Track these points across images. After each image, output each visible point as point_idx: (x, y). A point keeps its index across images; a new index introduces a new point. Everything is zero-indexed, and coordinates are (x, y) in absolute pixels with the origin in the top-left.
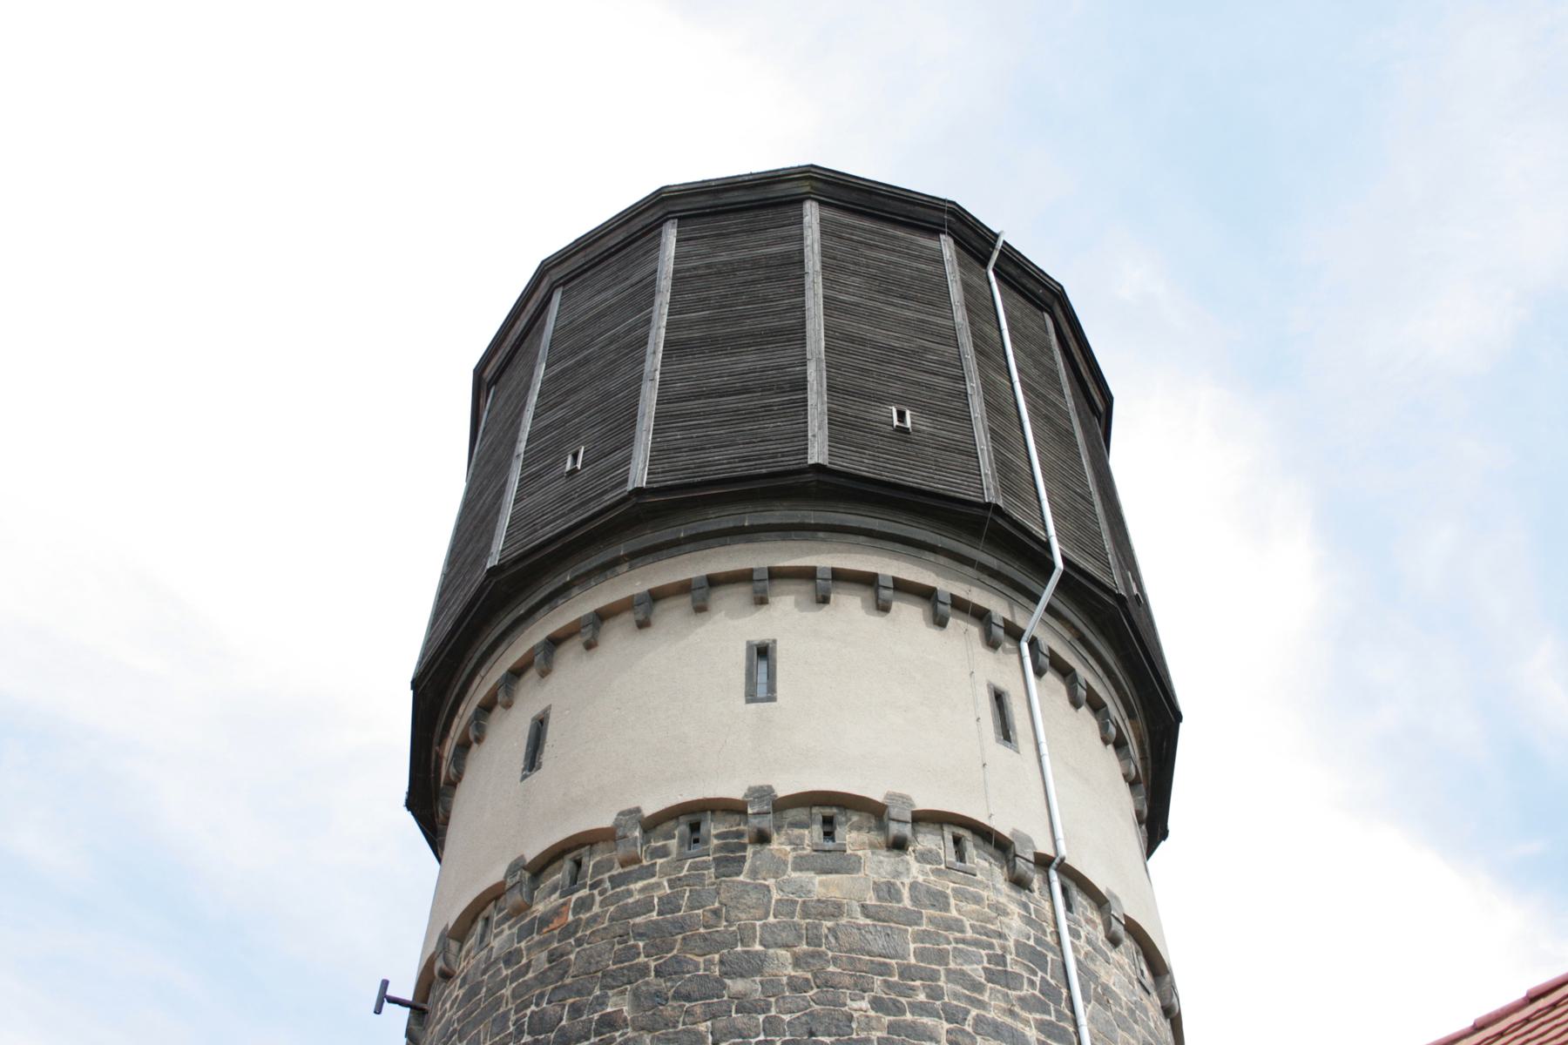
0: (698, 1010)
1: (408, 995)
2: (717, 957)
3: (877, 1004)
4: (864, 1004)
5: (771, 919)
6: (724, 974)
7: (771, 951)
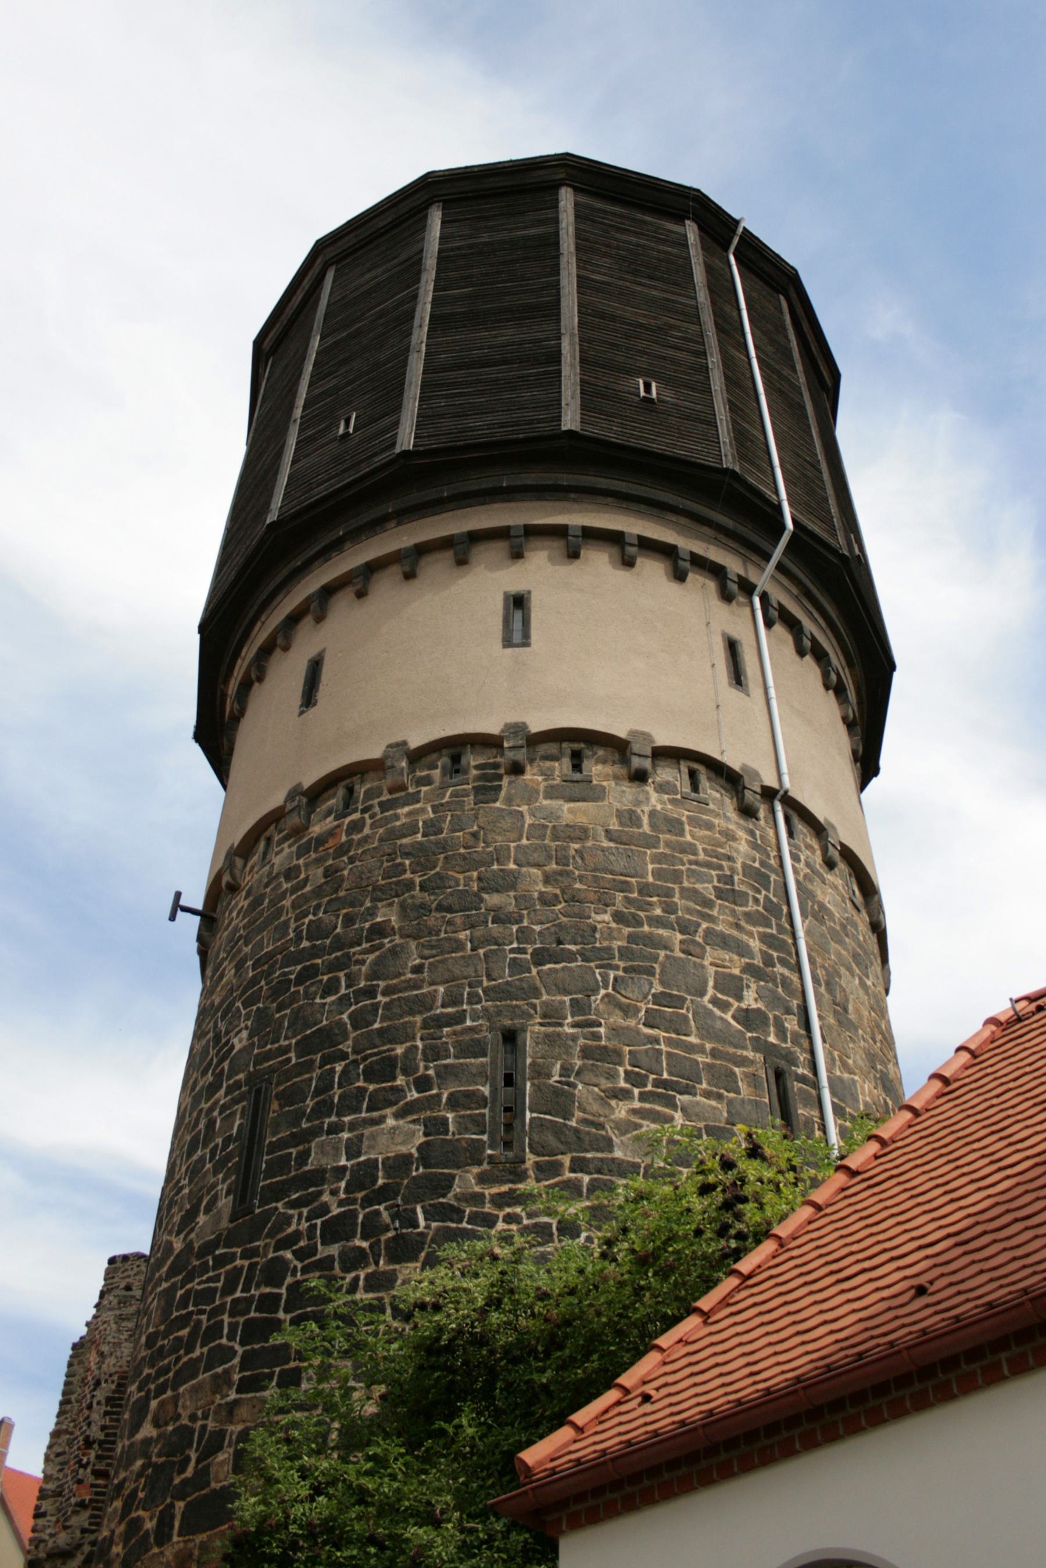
3: (618, 917)
4: (607, 917)
5: (524, 842)
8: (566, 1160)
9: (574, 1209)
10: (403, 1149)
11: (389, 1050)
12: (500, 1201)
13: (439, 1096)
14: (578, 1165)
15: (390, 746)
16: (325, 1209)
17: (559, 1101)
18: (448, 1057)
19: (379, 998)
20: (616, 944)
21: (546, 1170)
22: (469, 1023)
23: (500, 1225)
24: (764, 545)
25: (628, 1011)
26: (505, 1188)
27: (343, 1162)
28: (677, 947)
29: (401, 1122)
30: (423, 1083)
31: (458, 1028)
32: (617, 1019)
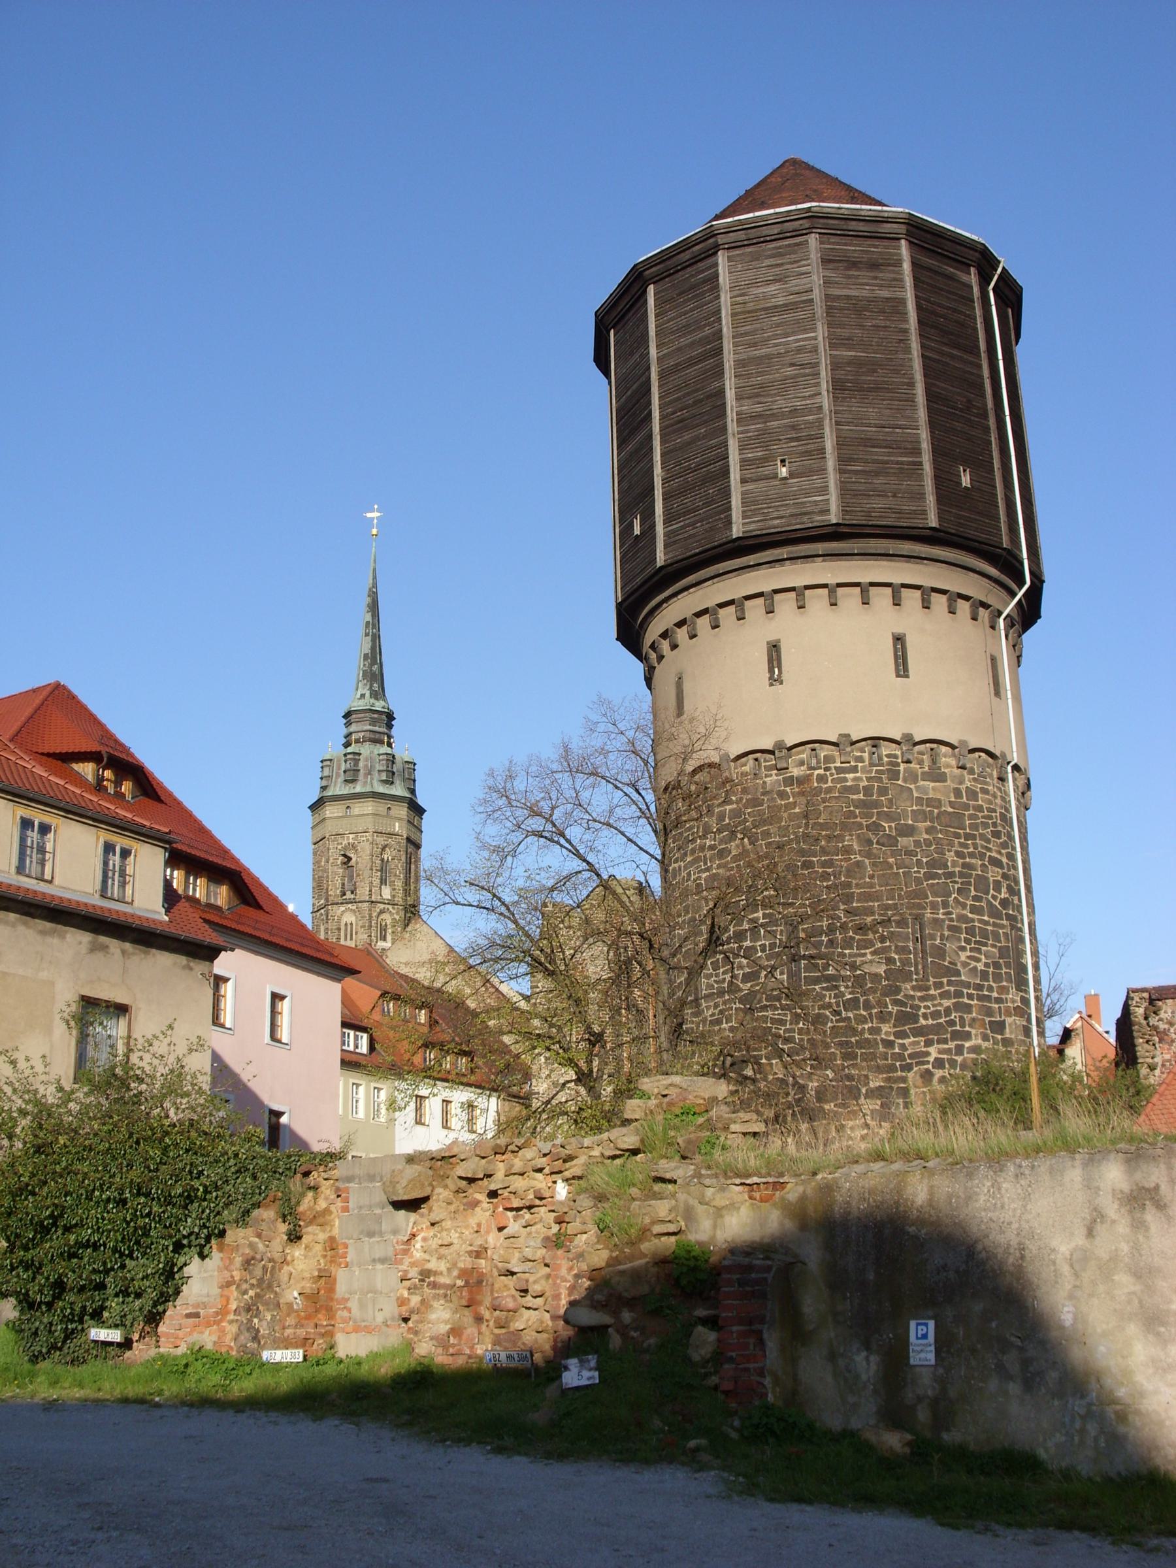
3: (958, 854)
4: (952, 853)
8: (945, 980)
9: (947, 1003)
12: (922, 999)
14: (950, 983)
20: (957, 869)
21: (938, 985)
23: (923, 1010)
24: (1014, 587)
25: (964, 906)
32: (959, 910)
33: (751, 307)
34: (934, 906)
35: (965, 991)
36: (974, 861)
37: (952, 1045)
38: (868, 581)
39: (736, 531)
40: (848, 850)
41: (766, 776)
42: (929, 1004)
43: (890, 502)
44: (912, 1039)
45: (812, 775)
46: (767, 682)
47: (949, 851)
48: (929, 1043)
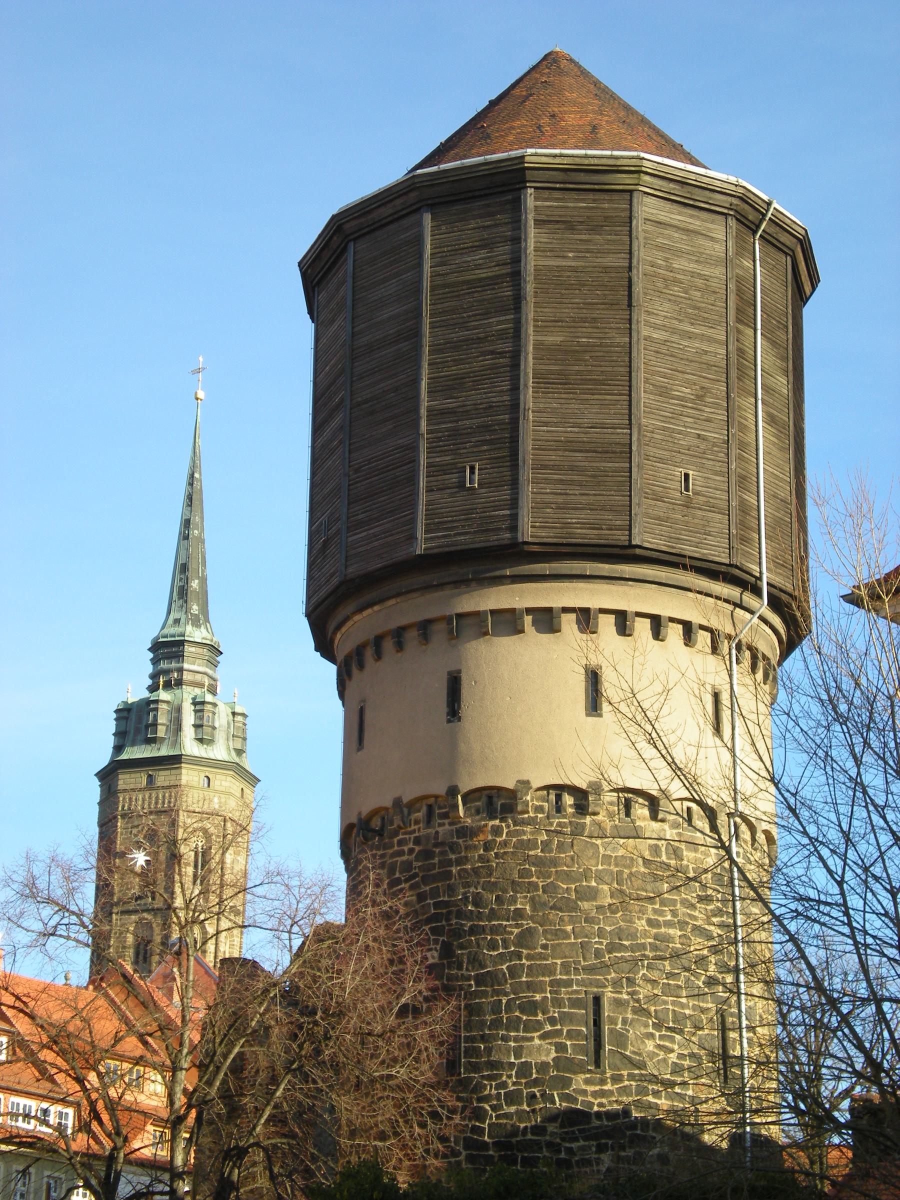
0: (566, 919)
1: (55, 1076)
2: (573, 886)
3: (650, 922)
4: (644, 922)
5: (600, 867)
6: (578, 899)
7: (601, 886)
8: (625, 1073)
10: (544, 1058)
11: (532, 996)
12: (595, 1094)
13: (561, 1030)
14: (631, 1077)
15: (518, 781)
16: (504, 1085)
17: (620, 1039)
18: (565, 1007)
19: (524, 961)
21: (616, 1079)
22: (575, 988)
26: (597, 1088)
27: (512, 1060)
28: (677, 940)
29: (543, 1042)
30: (552, 1021)
31: (570, 989)
33: (453, 278)
34: (616, 984)
35: (650, 1087)
36: (671, 931)
37: (629, 1153)
38: (561, 605)
39: (420, 548)
40: (519, 914)
41: (440, 825)
42: (604, 1100)
43: (585, 516)
44: (582, 1143)
45: (486, 825)
46: (444, 717)
47: (639, 918)
48: (601, 1149)
